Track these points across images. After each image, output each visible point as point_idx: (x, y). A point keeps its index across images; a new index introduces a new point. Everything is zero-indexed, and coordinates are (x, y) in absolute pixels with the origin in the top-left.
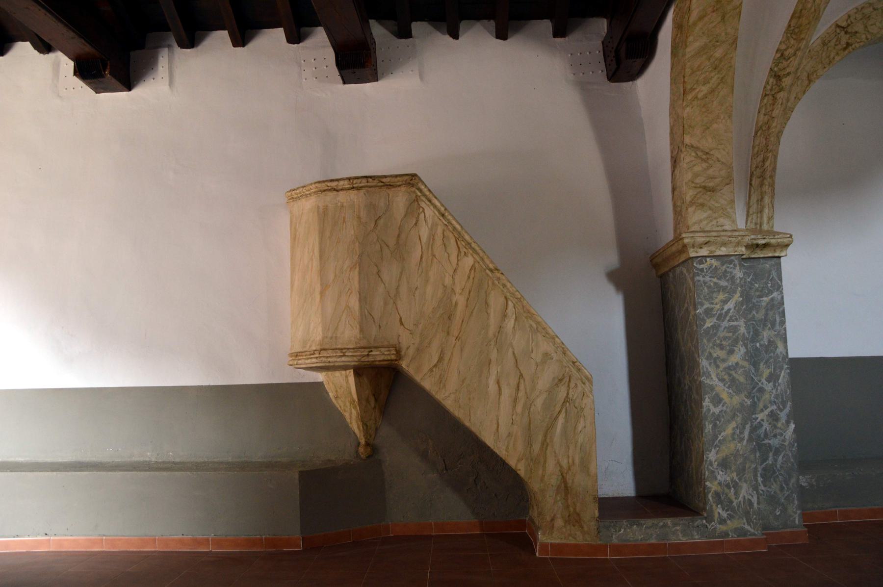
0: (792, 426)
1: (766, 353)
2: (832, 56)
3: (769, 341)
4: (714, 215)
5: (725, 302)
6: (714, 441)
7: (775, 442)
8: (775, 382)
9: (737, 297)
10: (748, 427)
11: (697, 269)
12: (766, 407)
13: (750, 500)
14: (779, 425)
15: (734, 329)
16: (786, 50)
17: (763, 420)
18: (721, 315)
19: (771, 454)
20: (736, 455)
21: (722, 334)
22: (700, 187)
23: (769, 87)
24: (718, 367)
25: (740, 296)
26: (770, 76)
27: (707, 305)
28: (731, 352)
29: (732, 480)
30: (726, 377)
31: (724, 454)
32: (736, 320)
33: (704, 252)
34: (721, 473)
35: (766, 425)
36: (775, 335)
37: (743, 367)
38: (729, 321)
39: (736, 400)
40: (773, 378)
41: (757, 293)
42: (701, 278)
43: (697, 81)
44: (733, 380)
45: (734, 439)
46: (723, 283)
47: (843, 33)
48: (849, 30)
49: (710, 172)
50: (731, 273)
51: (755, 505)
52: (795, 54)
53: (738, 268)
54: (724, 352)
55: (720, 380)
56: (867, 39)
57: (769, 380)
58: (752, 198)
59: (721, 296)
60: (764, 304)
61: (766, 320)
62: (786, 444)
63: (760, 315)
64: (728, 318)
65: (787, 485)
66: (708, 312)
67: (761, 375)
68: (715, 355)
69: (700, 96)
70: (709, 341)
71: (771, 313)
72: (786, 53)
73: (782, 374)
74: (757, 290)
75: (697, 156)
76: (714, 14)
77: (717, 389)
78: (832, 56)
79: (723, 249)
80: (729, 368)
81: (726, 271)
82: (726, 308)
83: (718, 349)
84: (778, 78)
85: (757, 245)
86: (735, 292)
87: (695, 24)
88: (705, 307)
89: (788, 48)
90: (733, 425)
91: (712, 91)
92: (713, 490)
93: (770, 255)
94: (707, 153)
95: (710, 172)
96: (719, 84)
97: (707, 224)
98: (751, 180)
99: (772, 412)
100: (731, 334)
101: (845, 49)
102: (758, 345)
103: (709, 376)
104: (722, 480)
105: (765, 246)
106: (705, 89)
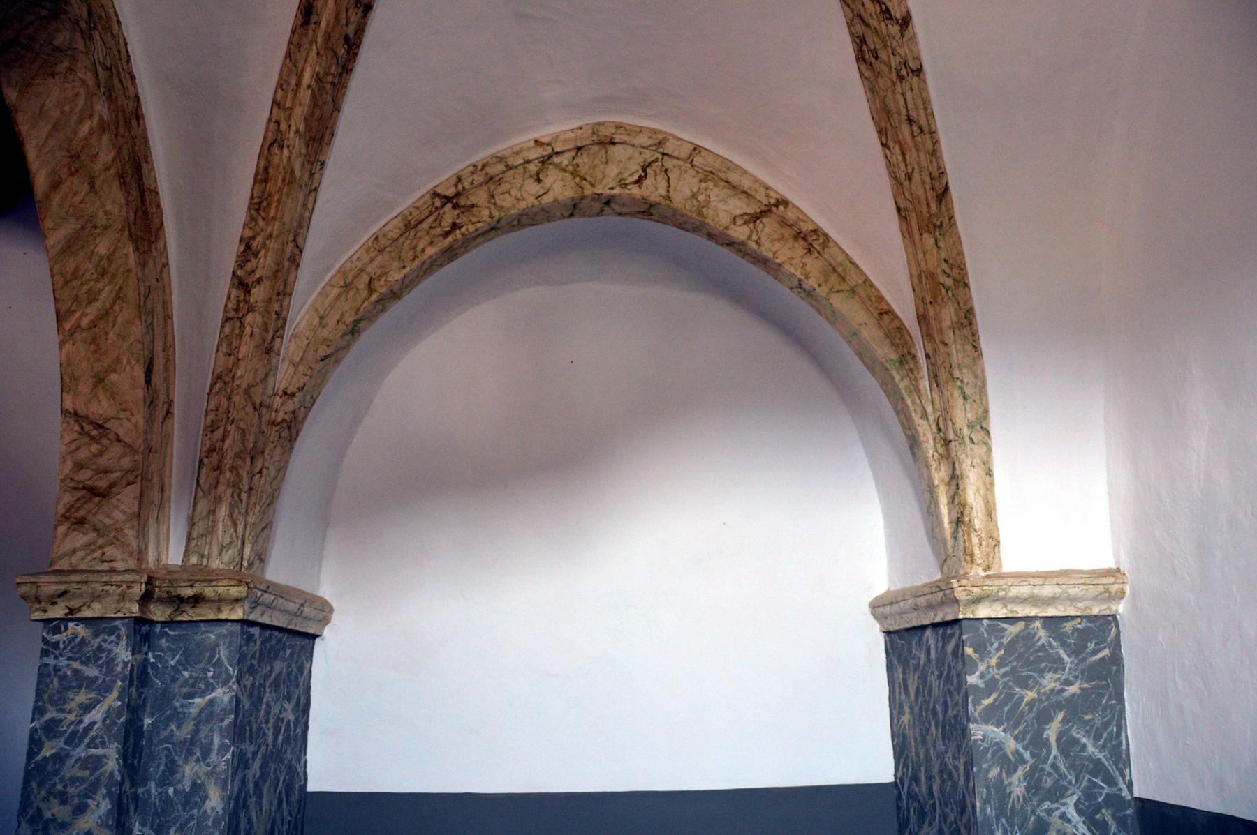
1: (185, 806)
2: (421, 246)
3: (194, 785)
4: (100, 541)
5: (87, 708)
9: (112, 700)
16: (253, 238)
18: (74, 733)
21: (69, 771)
22: (84, 488)
25: (119, 698)
28: (81, 809)
32: (103, 744)
38: (88, 746)
41: (185, 690)
46: (91, 671)
47: (449, 206)
48: (462, 202)
49: (103, 461)
50: (110, 651)
52: (264, 245)
53: (124, 642)
54: (68, 808)
56: (491, 216)
58: (199, 508)
59: (83, 697)
60: (194, 711)
61: (192, 742)
64: (87, 740)
68: (48, 815)
69: (85, 322)
71: (205, 730)
72: (254, 244)
74: (186, 681)
75: (83, 432)
76: (75, 180)
78: (421, 246)
79: (96, 605)
81: (100, 646)
82: (87, 719)
83: (56, 801)
86: (109, 689)
87: (47, 197)
88: (48, 716)
91: (105, 314)
93: (211, 617)
94: (101, 427)
95: (103, 461)
96: (114, 302)
97: (83, 559)
100: (88, 772)
101: (447, 234)
105: (197, 600)
106: (93, 310)
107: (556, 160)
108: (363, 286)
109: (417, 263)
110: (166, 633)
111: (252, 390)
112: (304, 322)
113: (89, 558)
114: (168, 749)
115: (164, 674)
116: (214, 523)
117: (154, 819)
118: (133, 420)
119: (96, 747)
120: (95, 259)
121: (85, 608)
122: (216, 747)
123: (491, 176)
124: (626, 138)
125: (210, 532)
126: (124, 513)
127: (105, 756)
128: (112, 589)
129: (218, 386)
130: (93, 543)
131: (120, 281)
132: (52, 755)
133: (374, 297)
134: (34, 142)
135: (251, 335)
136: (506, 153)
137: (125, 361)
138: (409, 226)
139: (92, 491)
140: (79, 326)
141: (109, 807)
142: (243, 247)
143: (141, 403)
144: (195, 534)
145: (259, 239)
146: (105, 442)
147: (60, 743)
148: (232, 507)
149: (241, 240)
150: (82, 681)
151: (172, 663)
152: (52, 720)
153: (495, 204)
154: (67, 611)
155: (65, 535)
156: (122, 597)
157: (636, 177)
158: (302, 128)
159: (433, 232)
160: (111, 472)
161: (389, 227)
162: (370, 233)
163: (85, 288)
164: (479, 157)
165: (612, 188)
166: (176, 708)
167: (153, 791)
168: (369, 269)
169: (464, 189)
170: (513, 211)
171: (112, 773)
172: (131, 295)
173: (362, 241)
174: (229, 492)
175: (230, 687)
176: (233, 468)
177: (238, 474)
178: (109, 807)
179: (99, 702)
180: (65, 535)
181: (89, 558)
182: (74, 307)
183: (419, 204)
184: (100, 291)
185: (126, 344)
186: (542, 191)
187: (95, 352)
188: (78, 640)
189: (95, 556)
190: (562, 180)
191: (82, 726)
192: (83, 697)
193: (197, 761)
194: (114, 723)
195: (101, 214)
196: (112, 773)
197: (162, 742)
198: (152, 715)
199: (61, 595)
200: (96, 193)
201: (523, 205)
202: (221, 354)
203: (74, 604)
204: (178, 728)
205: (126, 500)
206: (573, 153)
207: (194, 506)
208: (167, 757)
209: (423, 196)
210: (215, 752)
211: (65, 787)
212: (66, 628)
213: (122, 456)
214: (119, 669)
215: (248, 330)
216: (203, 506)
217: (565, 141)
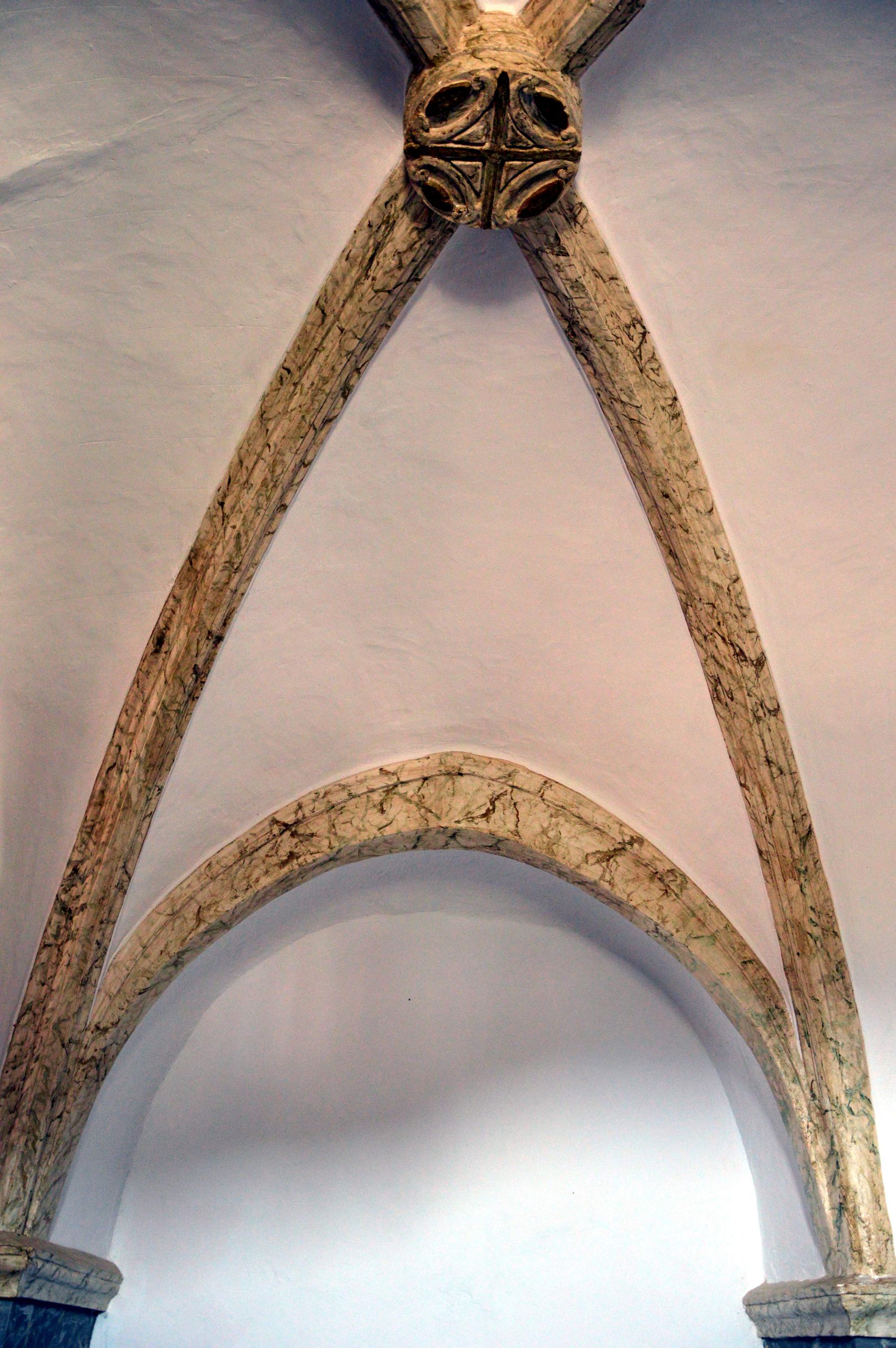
2: (254, 877)
16: (82, 862)
48: (301, 830)
56: (331, 847)
58: (33, 1203)
72: (82, 869)
78: (254, 877)
101: (284, 864)
108: (191, 915)
109: (250, 893)
111: (62, 1025)
112: (126, 951)
124: (474, 769)
133: (202, 927)
135: (68, 965)
136: (351, 781)
138: (245, 853)
142: (69, 871)
153: (336, 834)
157: (483, 811)
158: (143, 754)
159: (269, 860)
165: (458, 822)
168: (199, 897)
169: (304, 817)
170: (354, 843)
173: (194, 868)
174: (23, 1140)
176: (31, 1112)
177: (35, 1119)
190: (407, 811)
201: (364, 836)
202: (34, 982)
206: (419, 783)
215: (65, 958)
217: (411, 770)
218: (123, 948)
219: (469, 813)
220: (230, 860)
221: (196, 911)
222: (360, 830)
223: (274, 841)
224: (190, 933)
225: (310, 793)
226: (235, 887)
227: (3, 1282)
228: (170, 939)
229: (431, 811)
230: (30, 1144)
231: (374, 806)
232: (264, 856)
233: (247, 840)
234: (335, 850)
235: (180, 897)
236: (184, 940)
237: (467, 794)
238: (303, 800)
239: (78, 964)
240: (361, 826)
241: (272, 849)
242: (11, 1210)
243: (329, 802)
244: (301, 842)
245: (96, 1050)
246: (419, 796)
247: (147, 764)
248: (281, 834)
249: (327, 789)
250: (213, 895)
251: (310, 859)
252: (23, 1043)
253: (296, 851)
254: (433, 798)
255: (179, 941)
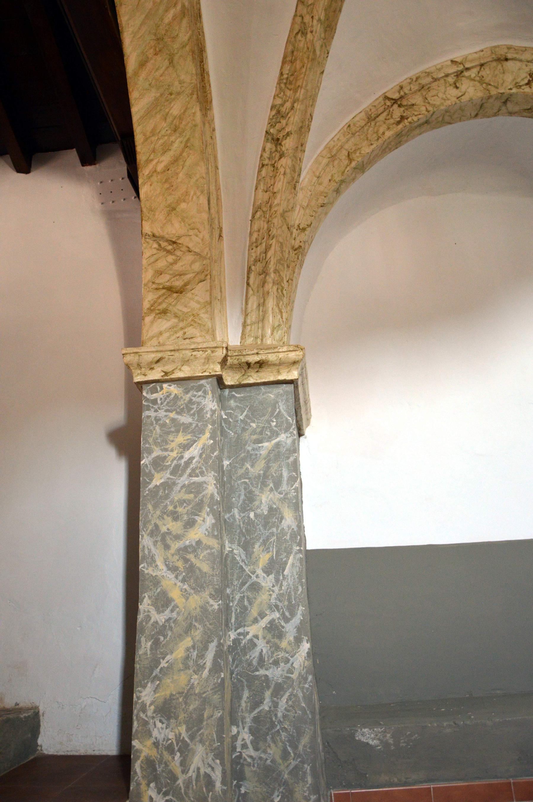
0: (306, 646)
1: (265, 526)
2: (381, 131)
3: (271, 509)
4: (181, 325)
5: (186, 447)
6: (152, 670)
7: (275, 674)
8: (278, 573)
9: (205, 439)
10: (212, 647)
11: (147, 400)
12: (262, 615)
13: (207, 776)
14: (284, 644)
15: (198, 488)
16: (282, 105)
17: (256, 637)
18: (177, 467)
19: (268, 694)
20: (187, 694)
21: (177, 495)
22: (163, 288)
23: (266, 155)
24: (167, 547)
25: (211, 438)
26: (267, 140)
27: (157, 452)
28: (190, 524)
29: (178, 737)
30: (180, 564)
31: (168, 693)
32: (202, 473)
33: (156, 375)
34: (159, 725)
35: (262, 645)
36: (280, 500)
37: (208, 547)
38: (190, 475)
39: (195, 601)
40: (275, 567)
41: (254, 437)
42: (151, 413)
43: (154, 151)
44: (191, 569)
45: (187, 667)
46: (185, 419)
48: (404, 102)
49: (178, 267)
51: (218, 785)
52: (292, 108)
53: (210, 395)
55: (169, 569)
57: (268, 571)
59: (181, 438)
60: (264, 452)
61: (265, 476)
62: (294, 676)
63: (257, 469)
64: (189, 471)
65: (295, 747)
66: (159, 464)
67: (255, 563)
68: (164, 529)
69: (160, 168)
70: (155, 507)
71: (274, 466)
72: (283, 109)
73: (290, 561)
74: (254, 432)
75: (160, 248)
76: (159, 58)
77: (164, 583)
78: (381, 131)
79: (186, 368)
80: (185, 549)
81: (191, 400)
82: (187, 455)
83: (169, 519)
84: (277, 142)
85: (249, 365)
86: (202, 432)
87: (136, 74)
89: (285, 102)
90: (188, 642)
91: (175, 161)
92: (143, 755)
93: (272, 379)
94: (174, 243)
95: (178, 267)
97: (169, 338)
98: (248, 278)
99: (272, 622)
100: (192, 496)
101: (399, 123)
102: (252, 515)
103: (153, 561)
104: (161, 737)
105: (261, 364)
106: (166, 159)
107: (466, 74)
108: (344, 157)
109: (380, 141)
110: (234, 396)
111: (286, 214)
112: (307, 180)
113: (174, 337)
114: (245, 483)
115: (235, 426)
116: (265, 312)
117: (240, 538)
118: (201, 236)
119: (197, 476)
120: (169, 120)
121: (177, 371)
122: (286, 479)
123: (423, 85)
124: (515, 56)
125: (262, 319)
126: (198, 302)
127: (205, 482)
128: (198, 354)
129: (258, 215)
130: (176, 326)
131: (188, 134)
132: (162, 484)
133: (353, 164)
134: (131, 30)
135: (285, 174)
136: (433, 69)
137: (192, 193)
138: (371, 118)
139: (170, 289)
140: (155, 171)
141: (213, 521)
142: (274, 112)
143: (206, 223)
144: (249, 322)
145: (288, 105)
146: (178, 253)
147: (167, 475)
148: (279, 299)
149: (273, 107)
150: (179, 428)
151: (242, 417)
152: (158, 457)
153: (429, 103)
154: (163, 374)
155: (152, 322)
156: (208, 360)
157: (526, 81)
158: (322, 17)
159: (387, 122)
160: (184, 274)
161: (357, 119)
162: (344, 123)
163: (161, 142)
164: (413, 73)
165: (511, 89)
166: (248, 451)
167: (237, 516)
168: (346, 147)
169: (405, 94)
170: (442, 108)
171: (212, 495)
172: (197, 143)
173: (339, 128)
174: (275, 288)
175: (291, 433)
176: (276, 271)
177: (280, 275)
178: (213, 521)
179: (195, 441)
180: (152, 322)
181: (174, 337)
182: (151, 158)
183: (376, 103)
184: (173, 142)
185: (193, 180)
186: (460, 94)
187: (168, 189)
188: (172, 396)
189: (178, 335)
190: (474, 86)
191: (183, 461)
192: (181, 438)
193: (271, 490)
194: (209, 457)
195: (176, 83)
196: (212, 495)
197: (240, 478)
198: (229, 458)
199: (158, 361)
200: (174, 67)
201: (448, 103)
202: (260, 191)
203: (169, 368)
204: (252, 466)
205: (200, 293)
206: (478, 68)
207: (247, 303)
208: (245, 489)
209: (377, 99)
210: (285, 483)
211: (175, 507)
212: (162, 388)
213: (193, 262)
214: (208, 416)
215: (282, 170)
216: (253, 302)
217: (472, 61)
218: (304, 179)
219: (517, 83)
220: (363, 123)
221: (347, 154)
222: (445, 100)
223: (388, 111)
224: (346, 168)
225: (406, 79)
226: (387, 121)
227: (287, 370)
228: (333, 172)
229: (490, 85)
230: (279, 291)
231: (450, 85)
232: (383, 119)
233: (371, 110)
234: (431, 112)
235: (334, 147)
236: (343, 172)
237: (513, 72)
238: (404, 84)
239: (291, 174)
240: (444, 97)
241: (388, 115)
242: (277, 331)
243: (420, 84)
244: (407, 109)
245: (301, 242)
246: (479, 77)
247: (326, 26)
248: (392, 105)
249: (418, 75)
250: (355, 145)
251: (415, 119)
252: (259, 231)
253: (405, 114)
254: (490, 76)
255: (340, 174)
